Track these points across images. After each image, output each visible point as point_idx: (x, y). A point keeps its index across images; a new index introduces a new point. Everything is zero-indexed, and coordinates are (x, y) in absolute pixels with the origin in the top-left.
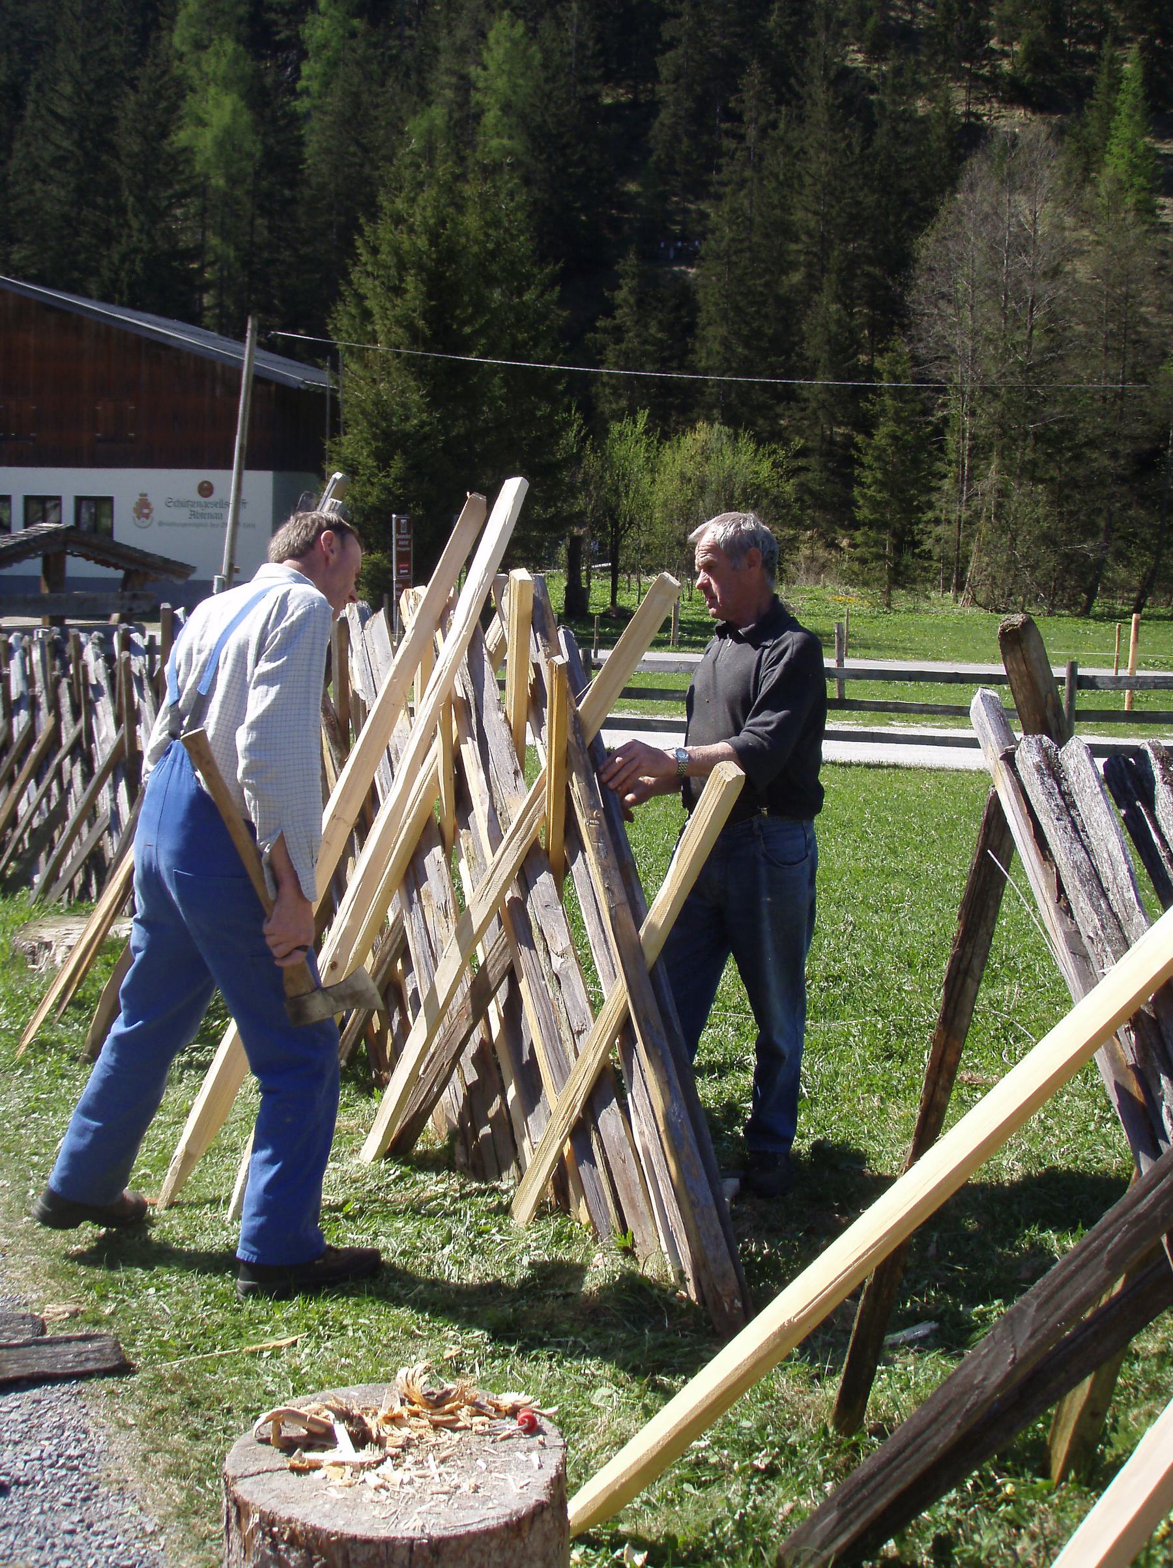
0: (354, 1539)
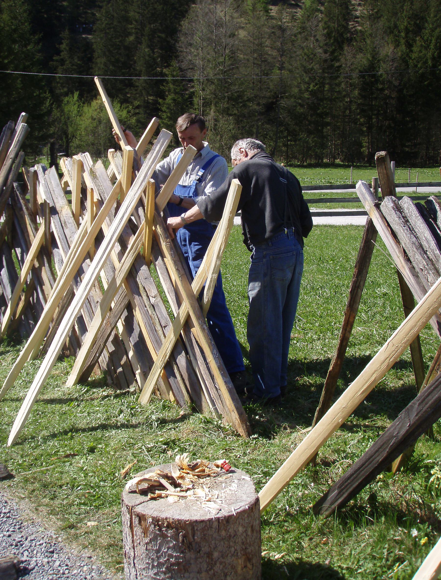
0: (196, 521)
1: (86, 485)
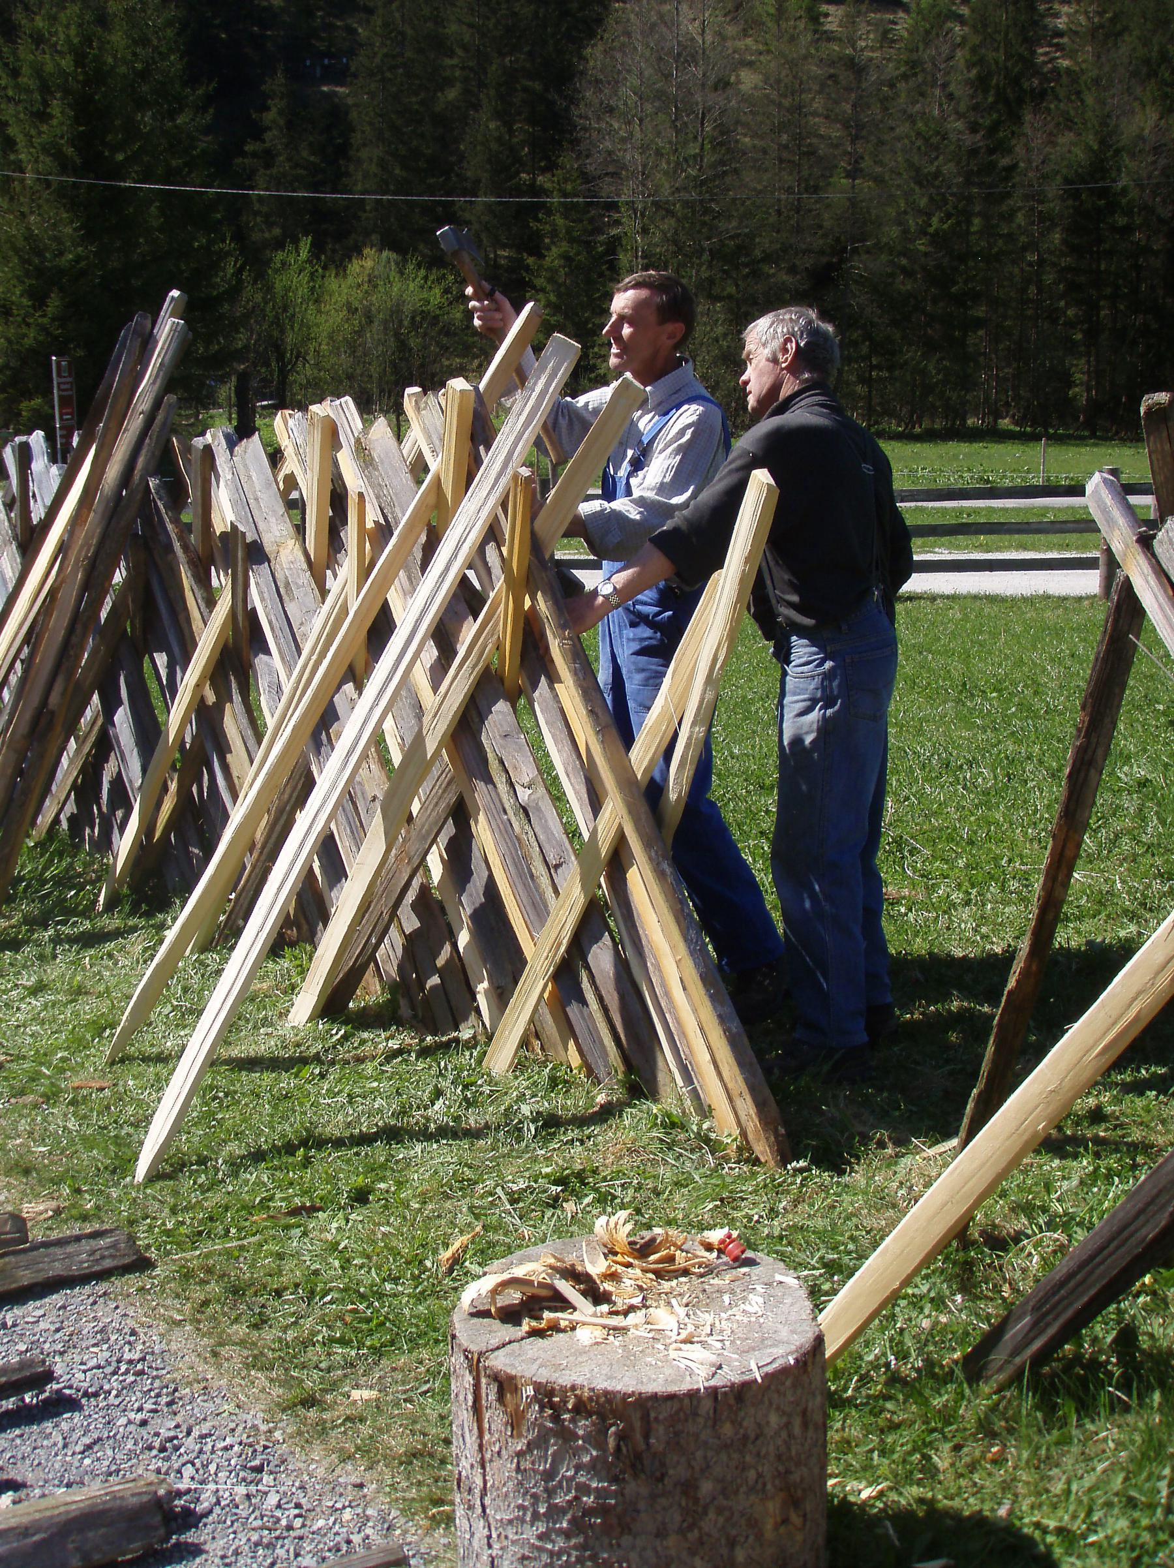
0: (655, 1397)
1: (345, 1290)
